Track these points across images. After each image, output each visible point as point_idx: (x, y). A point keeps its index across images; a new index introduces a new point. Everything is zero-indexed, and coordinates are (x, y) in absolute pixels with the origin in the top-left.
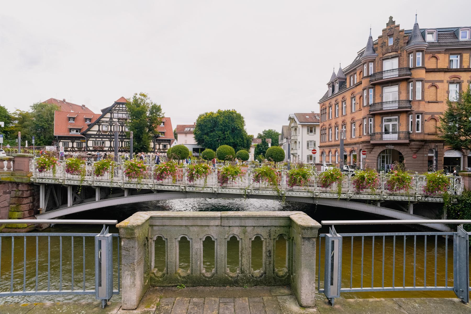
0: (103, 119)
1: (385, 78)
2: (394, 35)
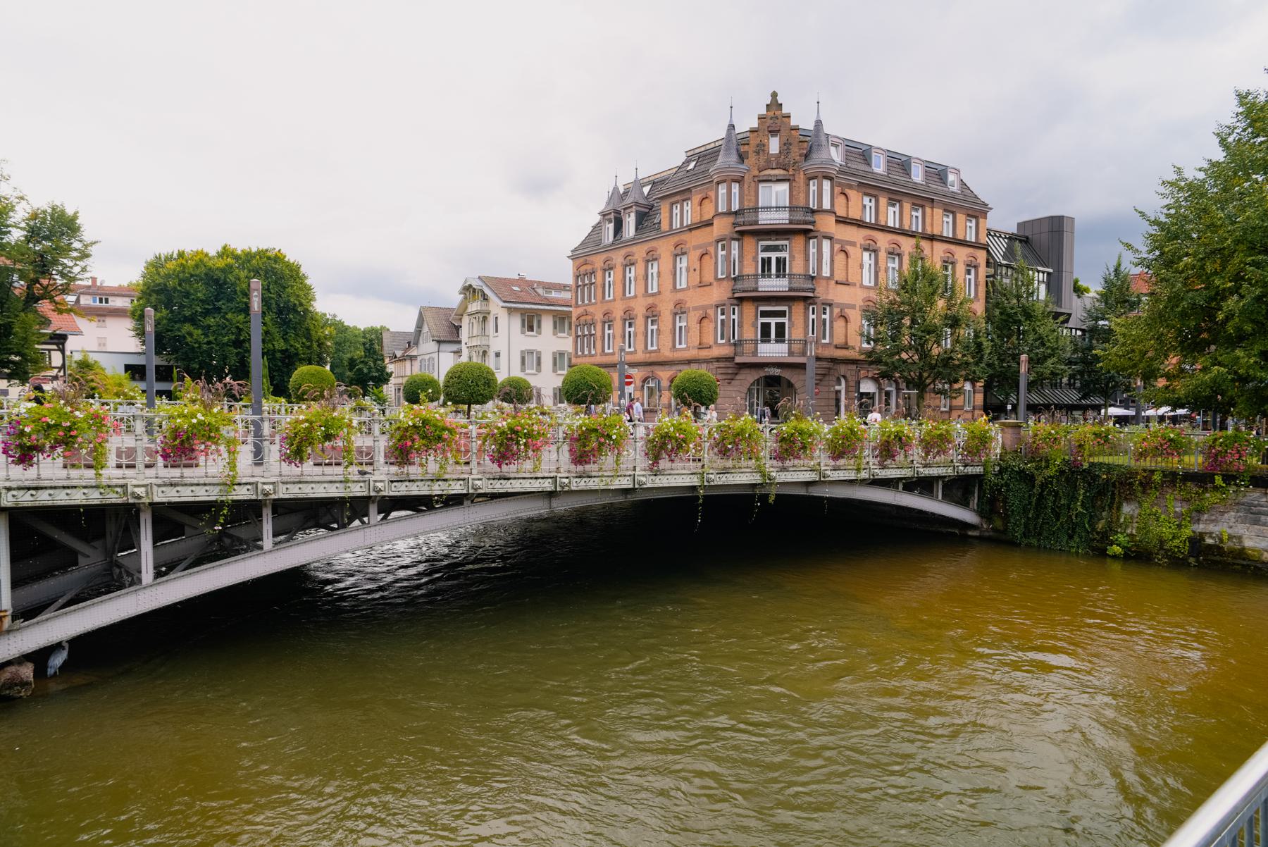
1: (763, 222)
2: (783, 133)
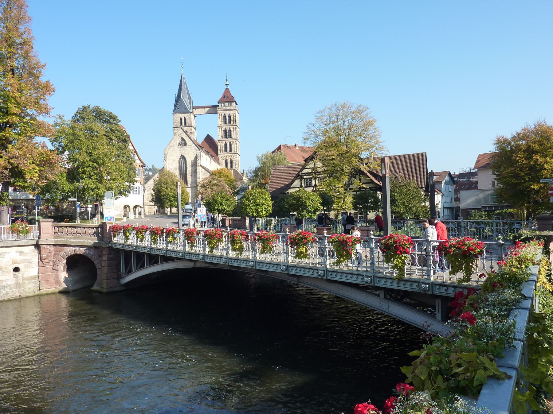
0: (305, 171)
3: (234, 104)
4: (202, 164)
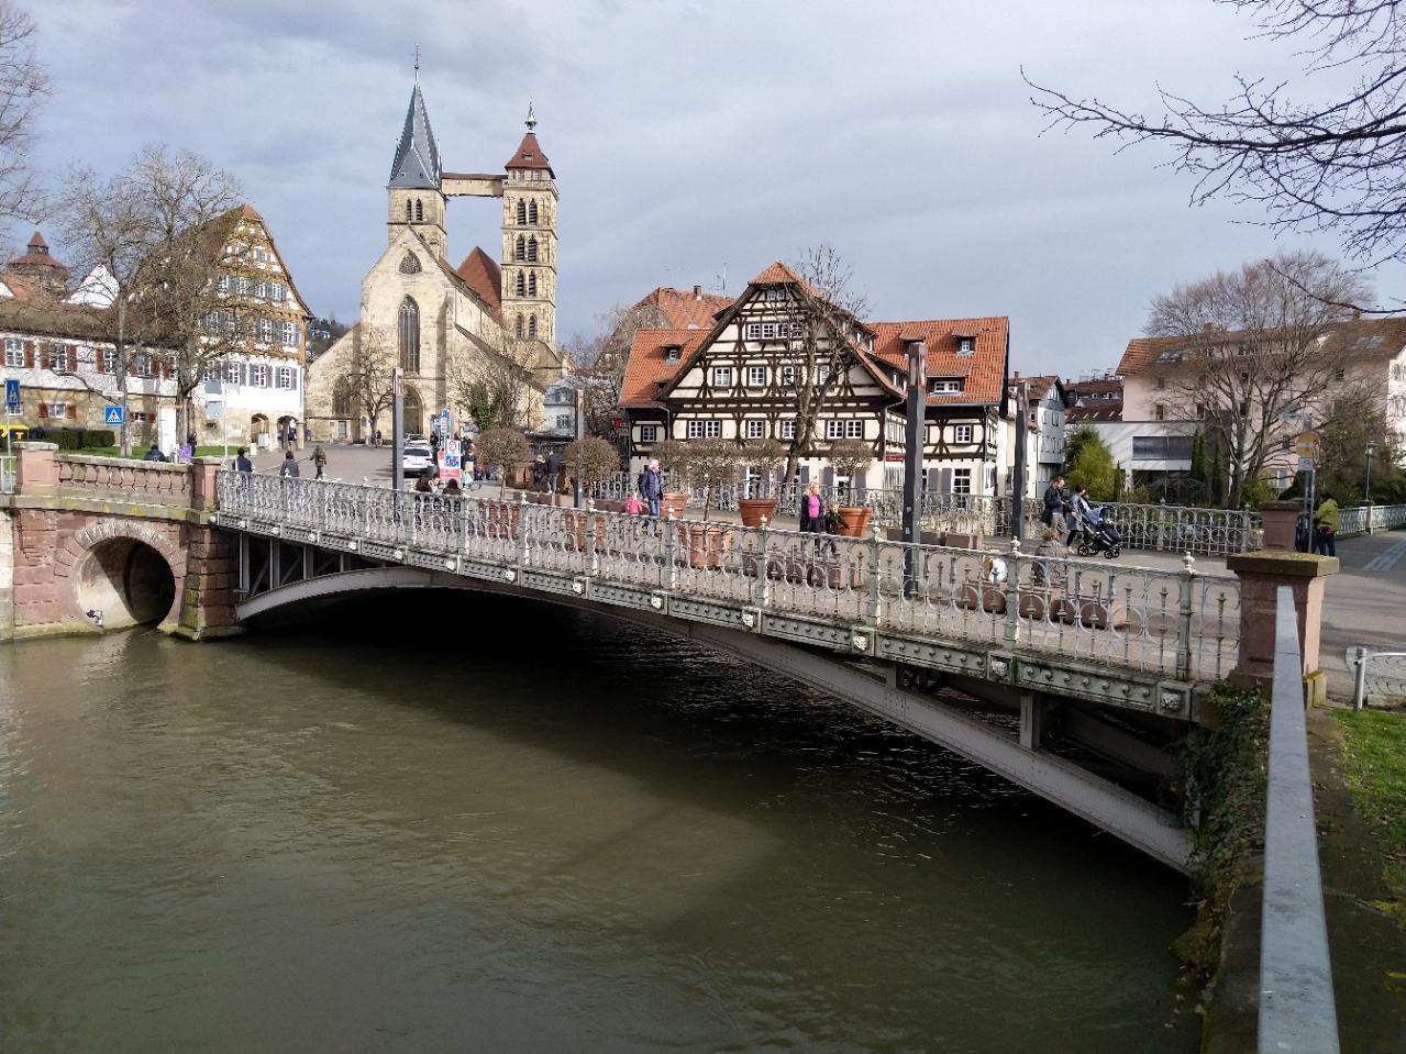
0: (715, 348)
3: (546, 175)
4: (458, 323)
